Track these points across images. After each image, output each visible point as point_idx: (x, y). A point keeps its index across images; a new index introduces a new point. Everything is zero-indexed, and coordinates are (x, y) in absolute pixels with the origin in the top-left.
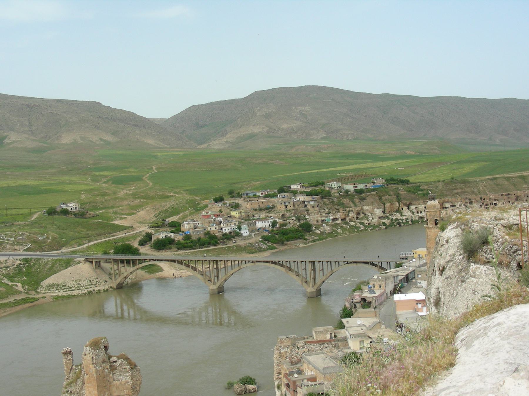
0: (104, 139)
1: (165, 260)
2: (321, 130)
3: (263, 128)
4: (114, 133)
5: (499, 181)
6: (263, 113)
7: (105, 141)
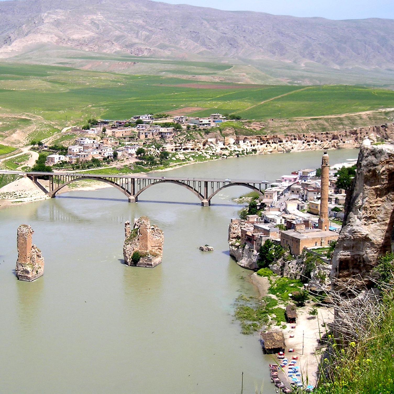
1: (172, 181)
3: (52, 37)
5: (321, 121)
6: (52, 20)
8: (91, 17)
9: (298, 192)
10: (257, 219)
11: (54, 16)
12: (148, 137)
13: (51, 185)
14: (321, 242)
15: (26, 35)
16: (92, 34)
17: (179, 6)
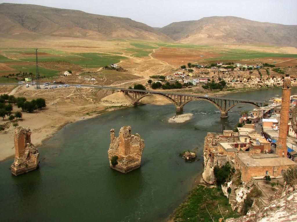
6: (207, 28)
8: (224, 27)
9: (279, 112)
10: (232, 134)
11: (208, 27)
13: (180, 100)
14: (273, 171)
16: (224, 34)
17: (264, 23)
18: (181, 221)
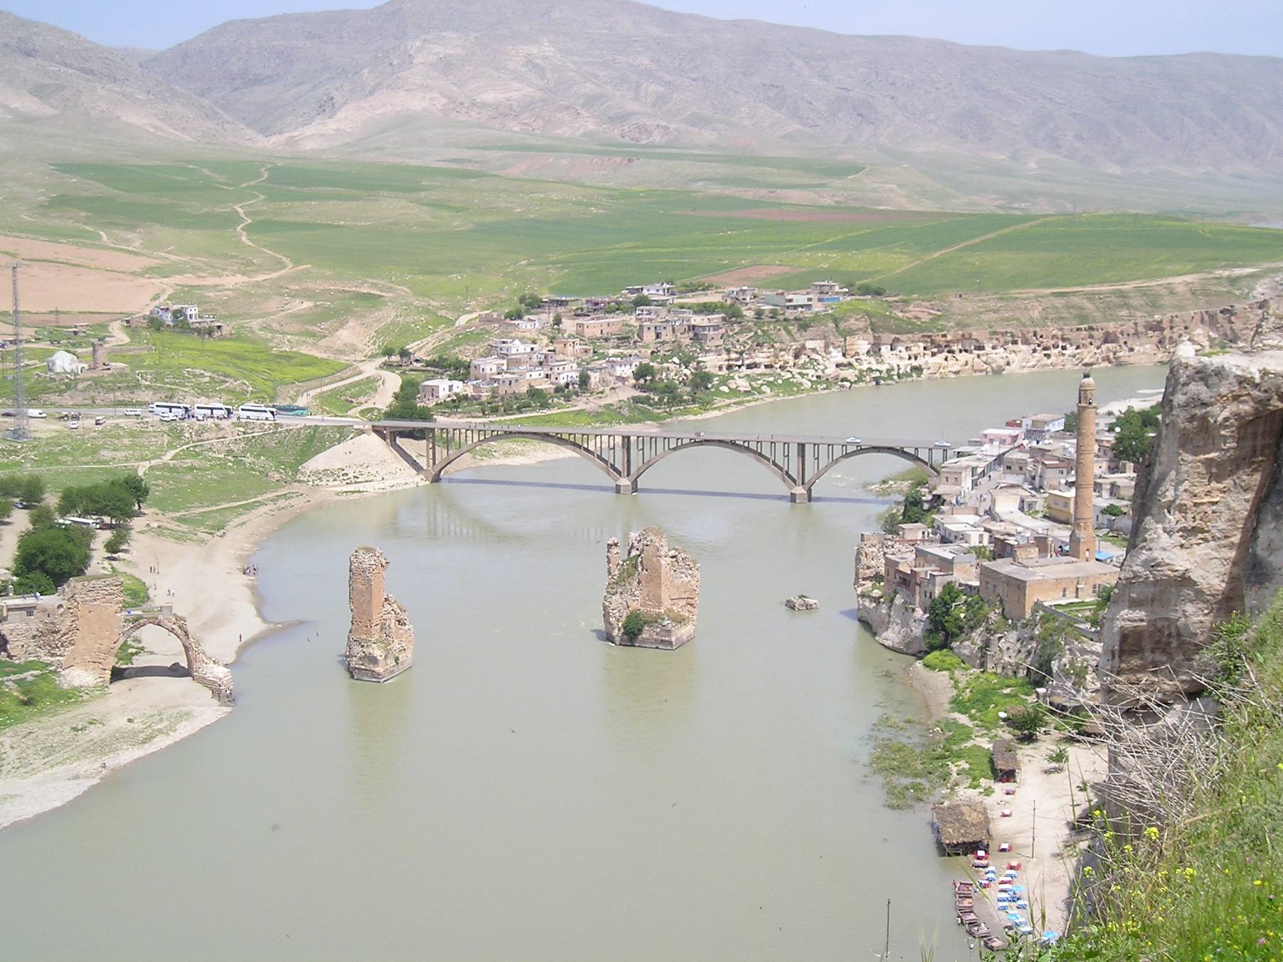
0: (14, 106)
2: (585, 114)
3: (432, 99)
4: (39, 91)
5: (1075, 300)
6: (431, 58)
7: (14, 112)
12: (664, 338)
15: (371, 93)
16: (528, 90)
17: (736, 24)
18: (1191, 943)
